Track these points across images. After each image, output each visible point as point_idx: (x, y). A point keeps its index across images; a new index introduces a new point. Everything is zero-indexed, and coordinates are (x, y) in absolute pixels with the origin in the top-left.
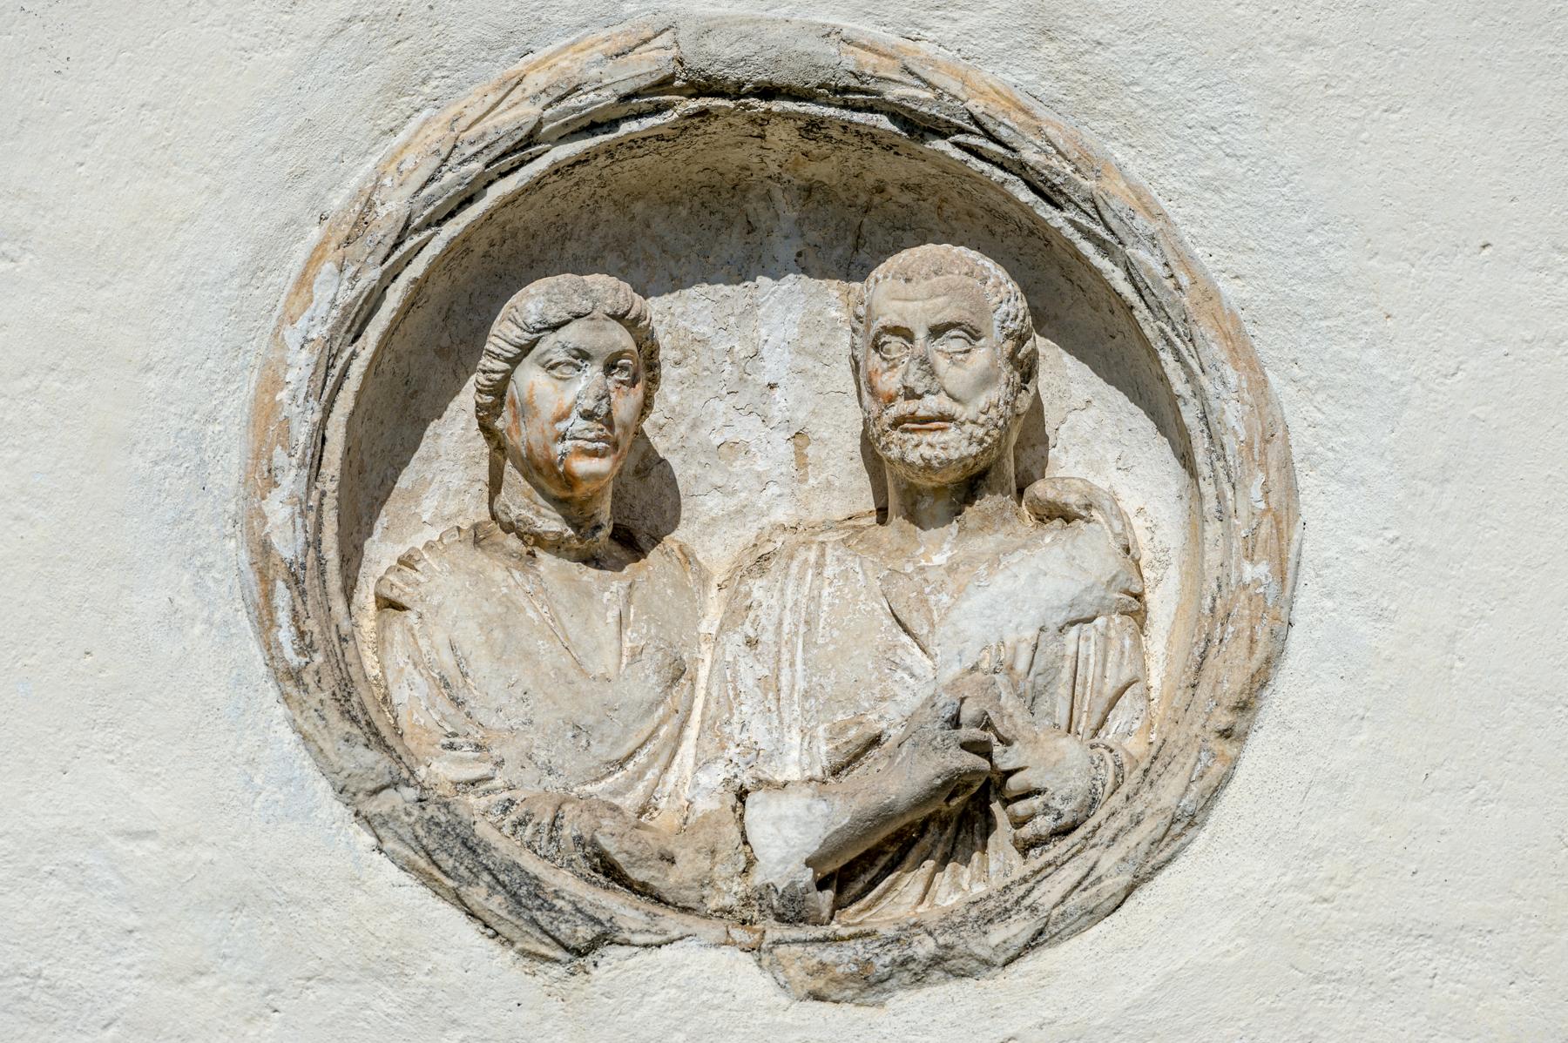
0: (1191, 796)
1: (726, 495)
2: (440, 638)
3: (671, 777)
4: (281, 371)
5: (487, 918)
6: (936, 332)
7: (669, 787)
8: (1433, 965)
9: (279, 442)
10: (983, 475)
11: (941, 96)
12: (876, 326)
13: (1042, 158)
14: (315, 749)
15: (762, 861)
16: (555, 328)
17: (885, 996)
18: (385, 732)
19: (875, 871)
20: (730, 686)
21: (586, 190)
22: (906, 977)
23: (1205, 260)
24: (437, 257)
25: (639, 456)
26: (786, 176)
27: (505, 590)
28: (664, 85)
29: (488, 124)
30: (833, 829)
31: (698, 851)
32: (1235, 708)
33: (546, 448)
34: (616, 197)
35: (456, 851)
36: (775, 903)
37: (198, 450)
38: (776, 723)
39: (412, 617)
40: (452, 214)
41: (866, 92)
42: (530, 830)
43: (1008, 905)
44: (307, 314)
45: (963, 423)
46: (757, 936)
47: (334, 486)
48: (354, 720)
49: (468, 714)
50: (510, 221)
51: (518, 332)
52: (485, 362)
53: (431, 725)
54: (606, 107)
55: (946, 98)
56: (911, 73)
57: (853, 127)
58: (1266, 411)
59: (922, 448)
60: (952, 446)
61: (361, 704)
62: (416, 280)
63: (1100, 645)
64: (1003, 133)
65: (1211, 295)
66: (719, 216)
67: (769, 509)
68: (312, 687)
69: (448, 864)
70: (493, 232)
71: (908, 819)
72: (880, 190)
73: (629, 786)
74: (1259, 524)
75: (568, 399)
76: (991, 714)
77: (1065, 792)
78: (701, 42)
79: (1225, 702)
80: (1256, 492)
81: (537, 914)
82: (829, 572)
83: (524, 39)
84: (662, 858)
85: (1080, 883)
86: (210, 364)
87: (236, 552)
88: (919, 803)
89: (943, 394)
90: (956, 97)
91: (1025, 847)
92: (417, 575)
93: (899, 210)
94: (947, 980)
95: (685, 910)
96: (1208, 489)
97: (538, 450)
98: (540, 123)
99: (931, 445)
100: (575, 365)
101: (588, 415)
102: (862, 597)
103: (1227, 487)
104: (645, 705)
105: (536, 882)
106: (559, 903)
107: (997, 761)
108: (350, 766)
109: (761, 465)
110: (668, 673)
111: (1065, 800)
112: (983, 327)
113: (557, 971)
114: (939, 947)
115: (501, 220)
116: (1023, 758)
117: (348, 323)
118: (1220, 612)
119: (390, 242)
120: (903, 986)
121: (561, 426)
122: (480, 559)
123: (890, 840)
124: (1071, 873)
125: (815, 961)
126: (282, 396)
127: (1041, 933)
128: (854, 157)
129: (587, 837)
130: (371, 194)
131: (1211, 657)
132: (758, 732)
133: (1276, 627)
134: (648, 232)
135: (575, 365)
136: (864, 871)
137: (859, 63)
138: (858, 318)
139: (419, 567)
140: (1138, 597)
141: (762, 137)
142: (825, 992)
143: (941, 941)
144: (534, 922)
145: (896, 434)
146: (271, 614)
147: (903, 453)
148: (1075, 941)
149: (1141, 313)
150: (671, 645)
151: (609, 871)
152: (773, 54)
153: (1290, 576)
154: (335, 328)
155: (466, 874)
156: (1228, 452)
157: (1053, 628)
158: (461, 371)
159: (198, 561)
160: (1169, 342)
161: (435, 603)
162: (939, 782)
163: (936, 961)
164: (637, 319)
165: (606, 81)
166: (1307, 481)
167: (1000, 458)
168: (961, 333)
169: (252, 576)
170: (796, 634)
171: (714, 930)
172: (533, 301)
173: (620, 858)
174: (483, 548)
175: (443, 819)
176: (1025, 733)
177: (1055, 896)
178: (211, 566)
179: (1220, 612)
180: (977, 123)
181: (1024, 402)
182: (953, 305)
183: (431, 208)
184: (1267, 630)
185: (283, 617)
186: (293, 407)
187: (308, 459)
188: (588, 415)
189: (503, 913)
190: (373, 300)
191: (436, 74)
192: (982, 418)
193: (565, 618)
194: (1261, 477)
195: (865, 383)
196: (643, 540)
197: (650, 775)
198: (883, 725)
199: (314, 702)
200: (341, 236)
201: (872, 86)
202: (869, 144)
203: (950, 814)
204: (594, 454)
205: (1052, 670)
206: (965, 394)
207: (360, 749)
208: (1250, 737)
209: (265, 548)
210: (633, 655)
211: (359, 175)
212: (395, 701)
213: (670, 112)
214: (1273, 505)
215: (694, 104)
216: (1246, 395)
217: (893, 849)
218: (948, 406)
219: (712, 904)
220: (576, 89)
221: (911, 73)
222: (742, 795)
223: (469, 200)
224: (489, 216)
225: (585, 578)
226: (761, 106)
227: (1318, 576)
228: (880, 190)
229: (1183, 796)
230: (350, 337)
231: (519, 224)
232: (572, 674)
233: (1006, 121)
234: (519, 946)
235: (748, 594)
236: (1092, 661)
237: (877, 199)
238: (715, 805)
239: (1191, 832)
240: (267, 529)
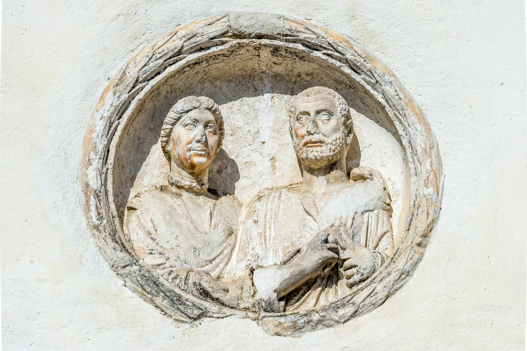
0: (408, 265)
1: (248, 179)
2: (148, 218)
3: (228, 267)
4: (94, 127)
5: (162, 308)
6: (318, 112)
7: (227, 271)
8: (492, 320)
9: (92, 150)
10: (335, 164)
11: (318, 37)
12: (297, 113)
13: (353, 57)
14: (103, 252)
15: (259, 291)
16: (187, 112)
17: (302, 334)
18: (128, 248)
19: (299, 296)
20: (248, 236)
21: (200, 76)
22: (309, 327)
23: (409, 90)
24: (148, 92)
25: (218, 166)
26: (267, 72)
27: (171, 204)
28: (223, 35)
29: (165, 47)
30: (283, 279)
31: (237, 287)
32: (422, 236)
33: (184, 154)
34: (210, 79)
35: (151, 285)
36: (264, 305)
37: (65, 153)
38: (264, 247)
39: (138, 212)
40: (153, 78)
41: (293, 36)
42: (178, 280)
43: (345, 302)
44: (103, 109)
45: (328, 144)
46: (257, 315)
47: (111, 166)
48: (117, 242)
49: (157, 243)
50: (174, 85)
51: (175, 114)
52: (164, 126)
53: (144, 247)
54: (205, 42)
55: (320, 37)
56: (308, 29)
57: (289, 50)
58: (431, 138)
59: (314, 153)
60: (324, 152)
61: (119, 237)
62: (140, 100)
63: (376, 219)
64: (340, 49)
65: (411, 101)
66: (245, 86)
67: (263, 183)
68: (102, 231)
69: (149, 290)
70: (167, 88)
71: (310, 277)
72: (299, 76)
73: (214, 270)
74: (429, 175)
75: (192, 136)
76: (338, 240)
77: (364, 267)
78: (237, 20)
79: (419, 234)
80: (428, 166)
81: (180, 306)
82: (282, 199)
83: (178, 20)
84: (224, 290)
85: (370, 295)
86: (70, 126)
87: (79, 188)
88: (316, 270)
89: (320, 134)
90: (323, 37)
91: (351, 286)
92: (141, 199)
93: (306, 83)
94: (324, 328)
95: (232, 308)
96: (411, 165)
97: (182, 155)
98: (183, 47)
99: (317, 151)
100: (194, 125)
101: (198, 141)
102: (294, 205)
103: (418, 164)
104: (219, 242)
105: (180, 297)
106: (187, 303)
107: (340, 255)
108: (115, 258)
109: (260, 169)
110: (227, 232)
111: (364, 269)
112: (334, 112)
113: (187, 326)
114: (321, 317)
115: (171, 83)
116: (350, 255)
117: (117, 112)
118: (417, 205)
119: (131, 85)
120: (309, 331)
121: (189, 146)
122: (163, 194)
123: (304, 285)
124: (367, 292)
125: (277, 322)
126: (94, 135)
127: (356, 311)
128: (290, 63)
129: (198, 282)
130: (125, 70)
131: (414, 220)
132: (258, 250)
133: (436, 209)
134: (221, 91)
135: (194, 125)
136: (295, 296)
137: (291, 26)
138: (292, 112)
139: (141, 196)
140: (389, 205)
141: (259, 56)
142: (281, 332)
143: (321, 314)
144: (178, 309)
145: (305, 149)
146: (88, 207)
147: (307, 155)
148: (368, 315)
149: (388, 108)
150: (228, 223)
151: (205, 294)
152: (261, 23)
153: (440, 192)
154: (112, 114)
155: (155, 293)
156: (418, 152)
157: (359, 213)
158: (157, 136)
159: (64, 190)
160: (397, 117)
161: (146, 207)
162: (320, 261)
163: (320, 322)
164: (215, 110)
165: (205, 33)
166: (445, 162)
167: (341, 159)
168: (327, 113)
169: (82, 195)
170: (271, 218)
171: (243, 313)
172: (180, 105)
173: (210, 290)
174: (164, 192)
175: (147, 275)
176: (350, 246)
177: (361, 299)
178: (69, 192)
179: (417, 205)
180: (332, 46)
181: (349, 140)
182: (324, 104)
183: (146, 75)
184: (433, 210)
185: (93, 208)
186: (97, 139)
187: (102, 157)
188: (198, 141)
189: (168, 306)
190: (126, 105)
191: (148, 32)
192: (334, 143)
193: (191, 213)
194: (430, 160)
195: (293, 133)
196: (219, 193)
197: (221, 266)
198: (301, 246)
199: (103, 236)
200: (115, 84)
201: (295, 34)
202: (295, 57)
203: (324, 275)
204: (201, 155)
205: (360, 226)
206: (329, 137)
207: (119, 252)
208: (428, 246)
209: (87, 185)
210: (215, 226)
211: (121, 65)
212: (132, 240)
213: (227, 44)
214: (434, 169)
215: (235, 41)
216: (424, 133)
217: (305, 288)
218: (322, 138)
219: (242, 306)
220: (195, 36)
221: (308, 29)
222: (252, 271)
223: (159, 73)
224: (166, 81)
225: (199, 201)
226: (258, 42)
227: (450, 192)
228: (299, 76)
229: (405, 265)
230: (118, 117)
231: (177, 86)
232: (194, 231)
233: (341, 45)
234: (173, 317)
235: (255, 207)
236: (373, 224)
237: (298, 79)
238: (243, 273)
239: (408, 278)
240: (88, 179)
